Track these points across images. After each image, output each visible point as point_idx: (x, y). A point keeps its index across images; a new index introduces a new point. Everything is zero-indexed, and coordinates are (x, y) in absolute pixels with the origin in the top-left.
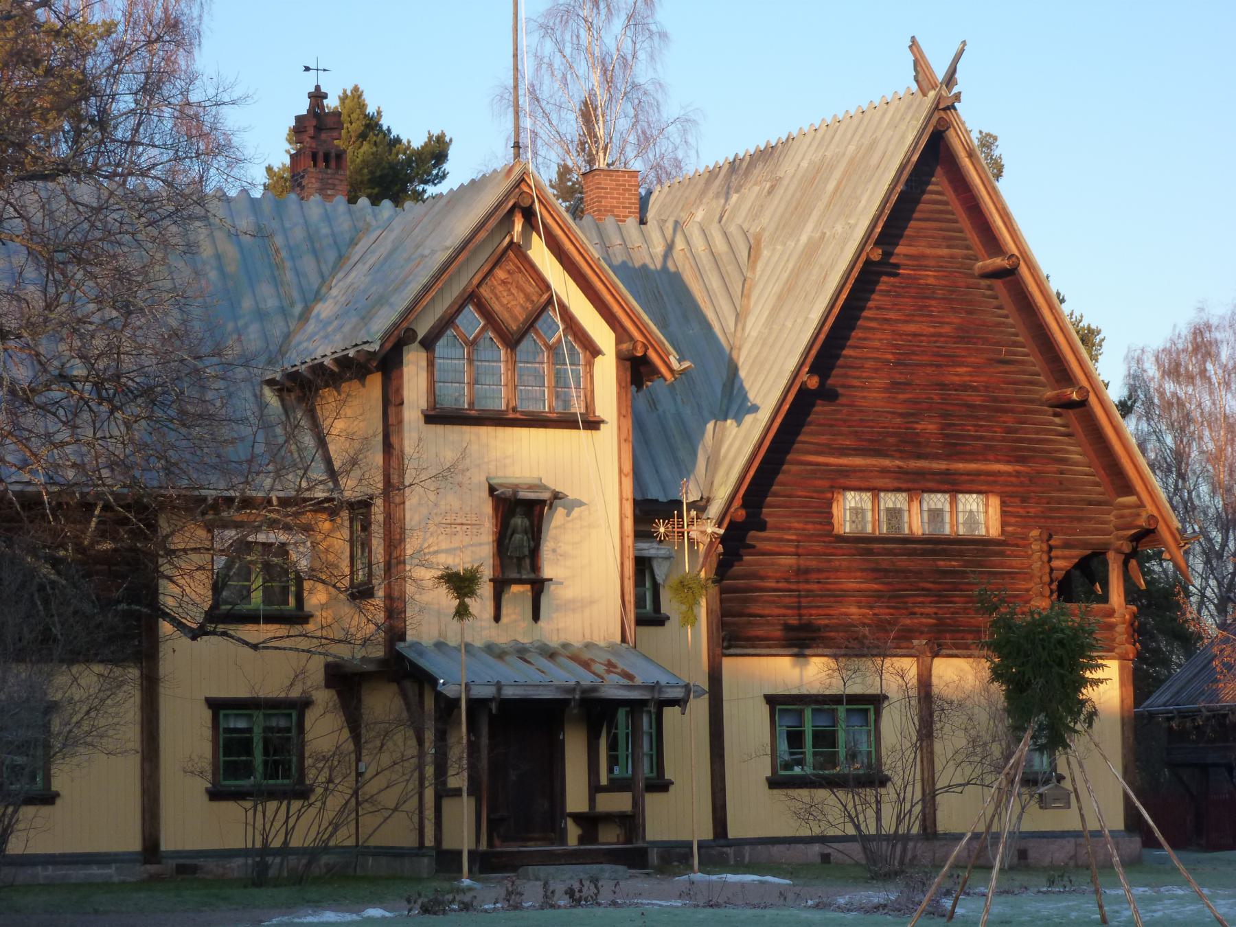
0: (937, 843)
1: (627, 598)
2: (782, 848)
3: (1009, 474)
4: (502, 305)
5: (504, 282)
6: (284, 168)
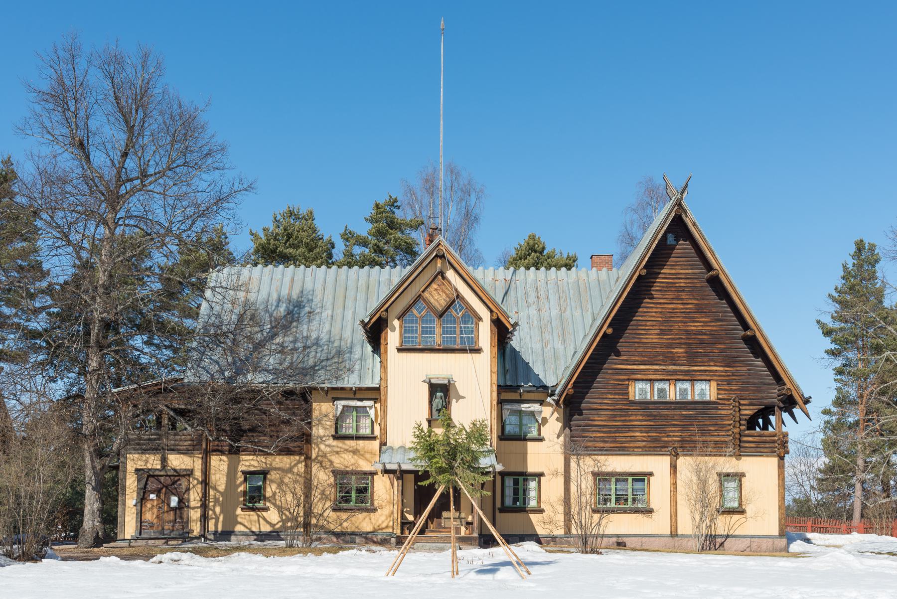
0: (676, 539)
1: (493, 427)
3: (722, 371)
5: (436, 290)
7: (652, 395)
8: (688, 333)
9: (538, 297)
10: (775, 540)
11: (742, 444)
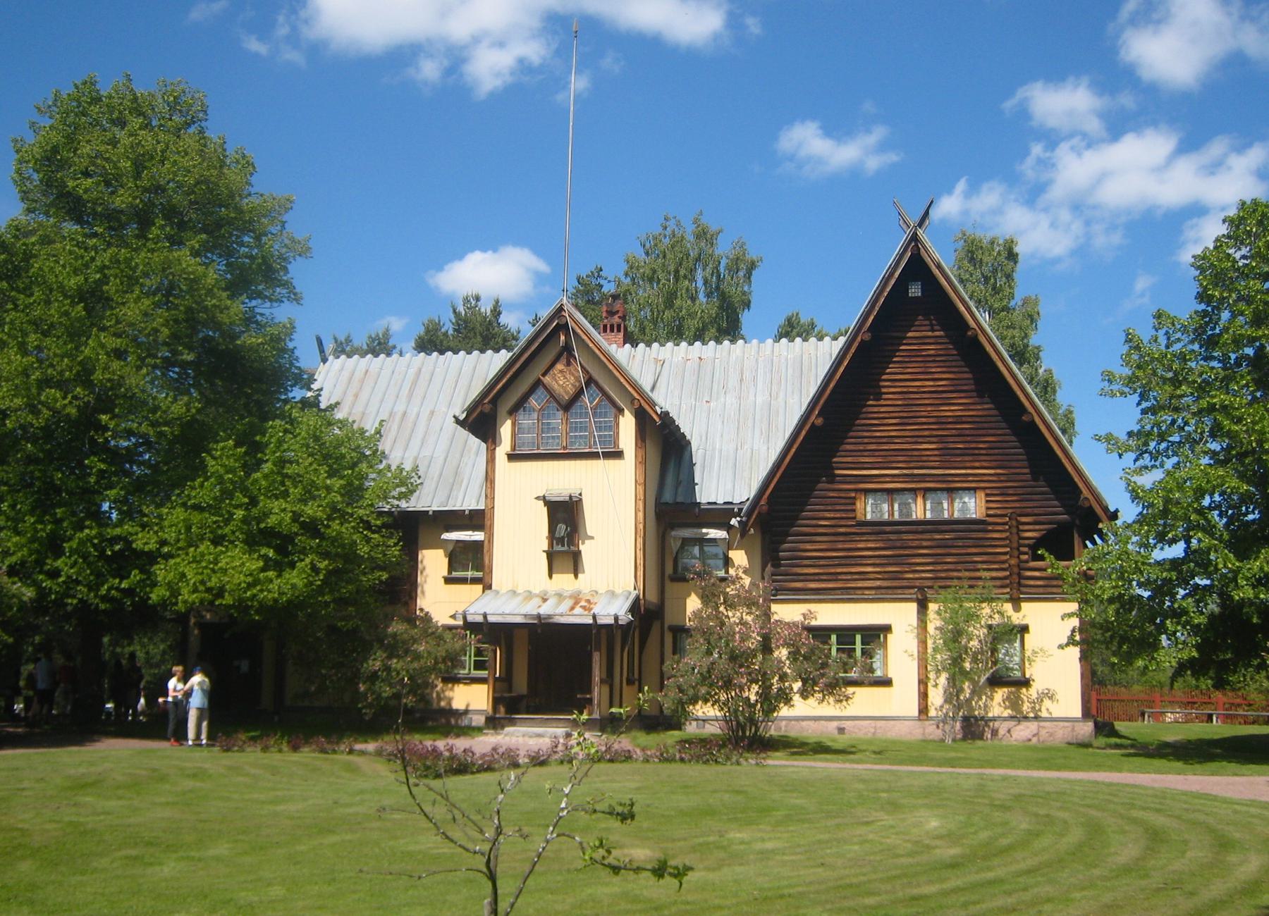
0: (927, 723)
2: (811, 723)
4: (559, 385)
5: (561, 371)
6: (450, 700)
7: (891, 513)
8: (941, 422)
9: (741, 380)
10: (1076, 724)
11: (1024, 582)
